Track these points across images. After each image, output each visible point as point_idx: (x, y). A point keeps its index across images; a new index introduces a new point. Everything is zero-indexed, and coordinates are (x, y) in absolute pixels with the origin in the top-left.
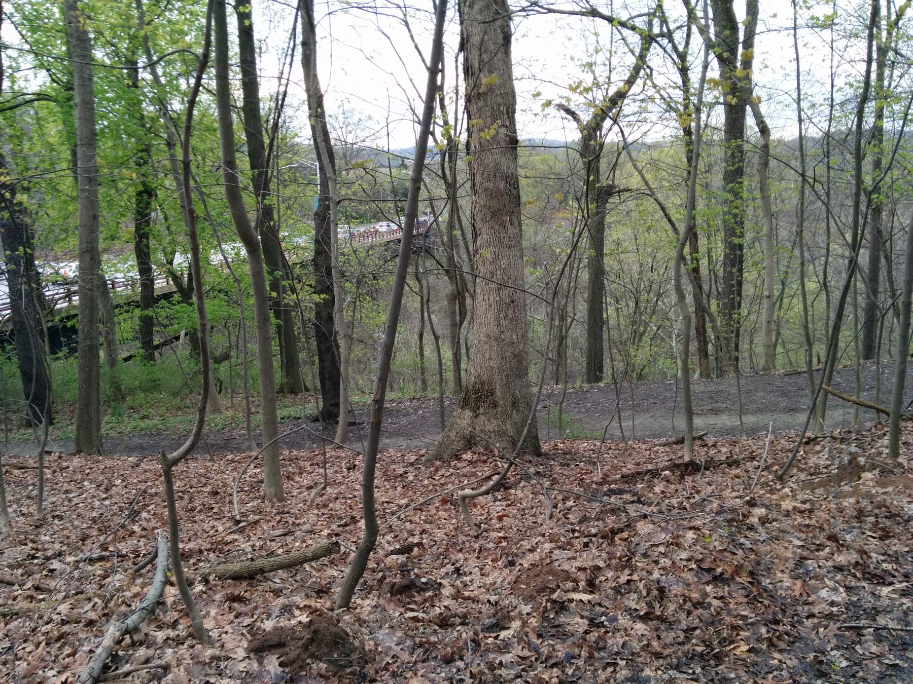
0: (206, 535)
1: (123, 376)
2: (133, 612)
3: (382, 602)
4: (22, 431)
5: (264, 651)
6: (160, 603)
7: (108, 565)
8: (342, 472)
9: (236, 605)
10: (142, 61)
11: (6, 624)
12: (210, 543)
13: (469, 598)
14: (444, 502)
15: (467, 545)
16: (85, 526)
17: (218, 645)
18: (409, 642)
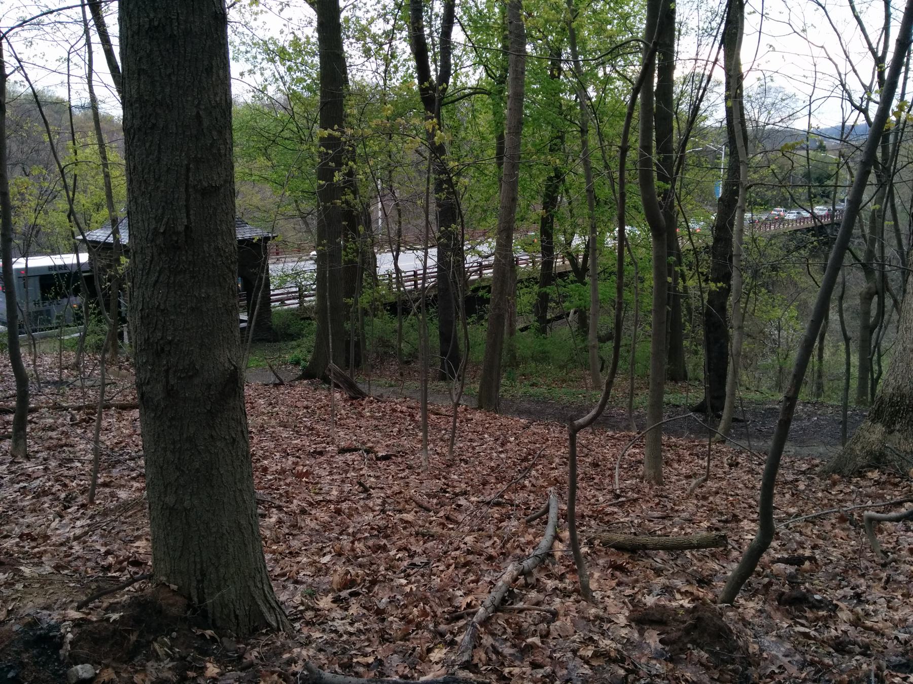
0: (587, 502)
1: (518, 345)
2: (528, 557)
3: (767, 607)
4: (435, 383)
5: (645, 624)
6: (549, 554)
7: (504, 511)
8: (723, 467)
9: (618, 573)
10: (566, 52)
11: (424, 543)
12: (591, 510)
13: (871, 629)
14: (842, 519)
15: (871, 571)
16: (485, 473)
17: (601, 606)
18: (798, 657)
